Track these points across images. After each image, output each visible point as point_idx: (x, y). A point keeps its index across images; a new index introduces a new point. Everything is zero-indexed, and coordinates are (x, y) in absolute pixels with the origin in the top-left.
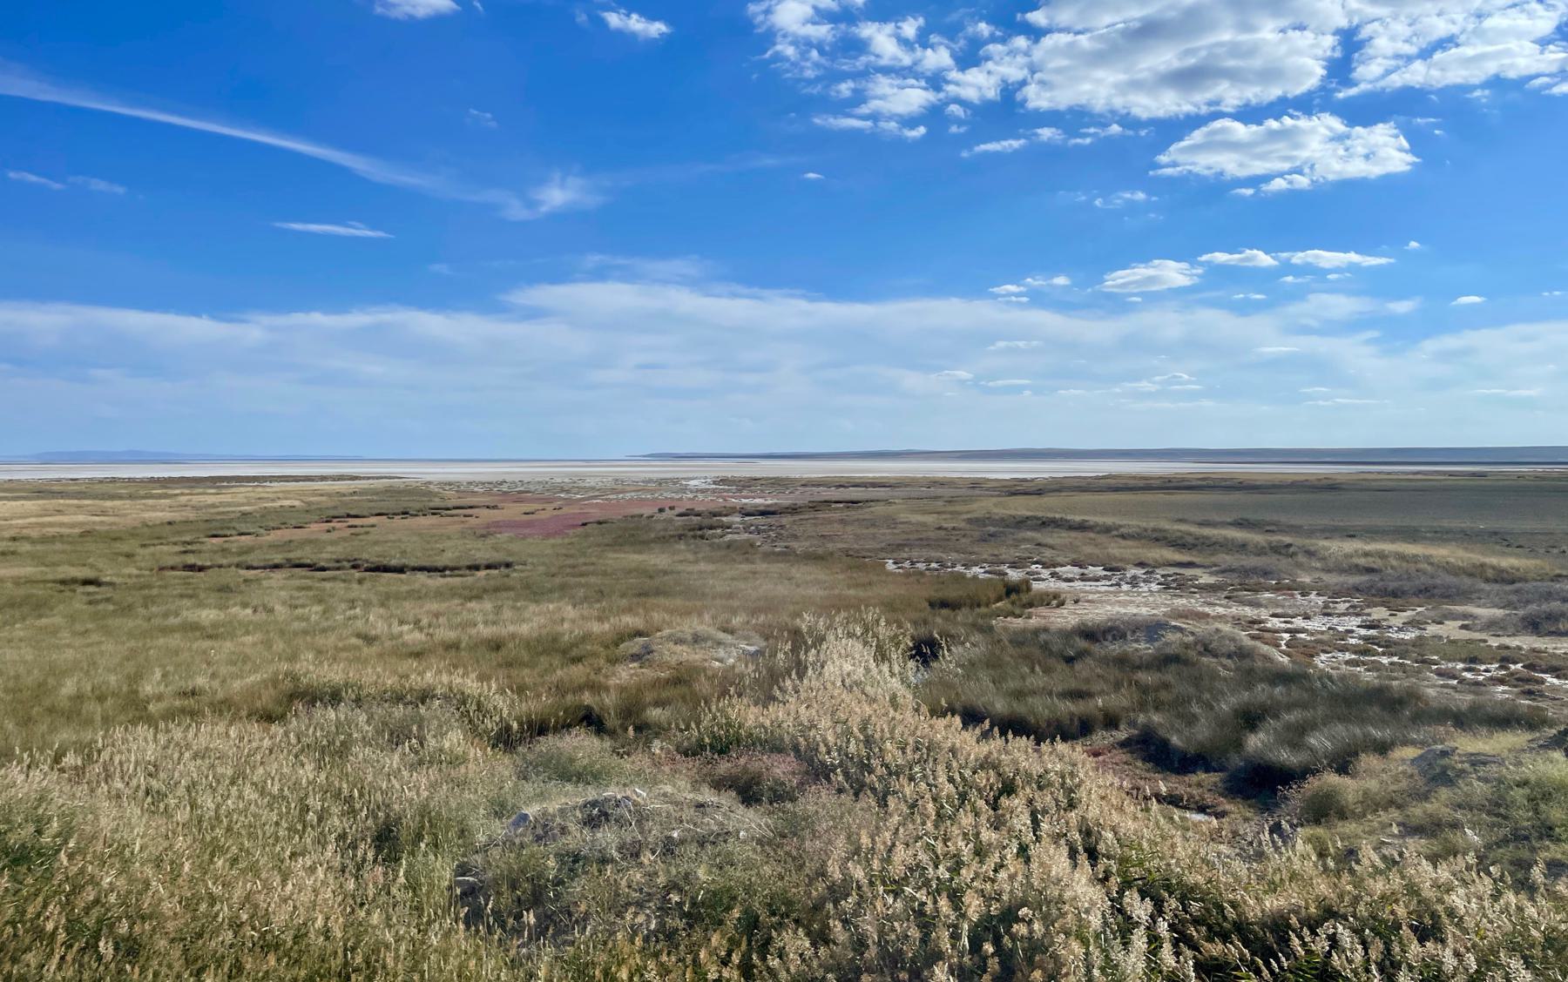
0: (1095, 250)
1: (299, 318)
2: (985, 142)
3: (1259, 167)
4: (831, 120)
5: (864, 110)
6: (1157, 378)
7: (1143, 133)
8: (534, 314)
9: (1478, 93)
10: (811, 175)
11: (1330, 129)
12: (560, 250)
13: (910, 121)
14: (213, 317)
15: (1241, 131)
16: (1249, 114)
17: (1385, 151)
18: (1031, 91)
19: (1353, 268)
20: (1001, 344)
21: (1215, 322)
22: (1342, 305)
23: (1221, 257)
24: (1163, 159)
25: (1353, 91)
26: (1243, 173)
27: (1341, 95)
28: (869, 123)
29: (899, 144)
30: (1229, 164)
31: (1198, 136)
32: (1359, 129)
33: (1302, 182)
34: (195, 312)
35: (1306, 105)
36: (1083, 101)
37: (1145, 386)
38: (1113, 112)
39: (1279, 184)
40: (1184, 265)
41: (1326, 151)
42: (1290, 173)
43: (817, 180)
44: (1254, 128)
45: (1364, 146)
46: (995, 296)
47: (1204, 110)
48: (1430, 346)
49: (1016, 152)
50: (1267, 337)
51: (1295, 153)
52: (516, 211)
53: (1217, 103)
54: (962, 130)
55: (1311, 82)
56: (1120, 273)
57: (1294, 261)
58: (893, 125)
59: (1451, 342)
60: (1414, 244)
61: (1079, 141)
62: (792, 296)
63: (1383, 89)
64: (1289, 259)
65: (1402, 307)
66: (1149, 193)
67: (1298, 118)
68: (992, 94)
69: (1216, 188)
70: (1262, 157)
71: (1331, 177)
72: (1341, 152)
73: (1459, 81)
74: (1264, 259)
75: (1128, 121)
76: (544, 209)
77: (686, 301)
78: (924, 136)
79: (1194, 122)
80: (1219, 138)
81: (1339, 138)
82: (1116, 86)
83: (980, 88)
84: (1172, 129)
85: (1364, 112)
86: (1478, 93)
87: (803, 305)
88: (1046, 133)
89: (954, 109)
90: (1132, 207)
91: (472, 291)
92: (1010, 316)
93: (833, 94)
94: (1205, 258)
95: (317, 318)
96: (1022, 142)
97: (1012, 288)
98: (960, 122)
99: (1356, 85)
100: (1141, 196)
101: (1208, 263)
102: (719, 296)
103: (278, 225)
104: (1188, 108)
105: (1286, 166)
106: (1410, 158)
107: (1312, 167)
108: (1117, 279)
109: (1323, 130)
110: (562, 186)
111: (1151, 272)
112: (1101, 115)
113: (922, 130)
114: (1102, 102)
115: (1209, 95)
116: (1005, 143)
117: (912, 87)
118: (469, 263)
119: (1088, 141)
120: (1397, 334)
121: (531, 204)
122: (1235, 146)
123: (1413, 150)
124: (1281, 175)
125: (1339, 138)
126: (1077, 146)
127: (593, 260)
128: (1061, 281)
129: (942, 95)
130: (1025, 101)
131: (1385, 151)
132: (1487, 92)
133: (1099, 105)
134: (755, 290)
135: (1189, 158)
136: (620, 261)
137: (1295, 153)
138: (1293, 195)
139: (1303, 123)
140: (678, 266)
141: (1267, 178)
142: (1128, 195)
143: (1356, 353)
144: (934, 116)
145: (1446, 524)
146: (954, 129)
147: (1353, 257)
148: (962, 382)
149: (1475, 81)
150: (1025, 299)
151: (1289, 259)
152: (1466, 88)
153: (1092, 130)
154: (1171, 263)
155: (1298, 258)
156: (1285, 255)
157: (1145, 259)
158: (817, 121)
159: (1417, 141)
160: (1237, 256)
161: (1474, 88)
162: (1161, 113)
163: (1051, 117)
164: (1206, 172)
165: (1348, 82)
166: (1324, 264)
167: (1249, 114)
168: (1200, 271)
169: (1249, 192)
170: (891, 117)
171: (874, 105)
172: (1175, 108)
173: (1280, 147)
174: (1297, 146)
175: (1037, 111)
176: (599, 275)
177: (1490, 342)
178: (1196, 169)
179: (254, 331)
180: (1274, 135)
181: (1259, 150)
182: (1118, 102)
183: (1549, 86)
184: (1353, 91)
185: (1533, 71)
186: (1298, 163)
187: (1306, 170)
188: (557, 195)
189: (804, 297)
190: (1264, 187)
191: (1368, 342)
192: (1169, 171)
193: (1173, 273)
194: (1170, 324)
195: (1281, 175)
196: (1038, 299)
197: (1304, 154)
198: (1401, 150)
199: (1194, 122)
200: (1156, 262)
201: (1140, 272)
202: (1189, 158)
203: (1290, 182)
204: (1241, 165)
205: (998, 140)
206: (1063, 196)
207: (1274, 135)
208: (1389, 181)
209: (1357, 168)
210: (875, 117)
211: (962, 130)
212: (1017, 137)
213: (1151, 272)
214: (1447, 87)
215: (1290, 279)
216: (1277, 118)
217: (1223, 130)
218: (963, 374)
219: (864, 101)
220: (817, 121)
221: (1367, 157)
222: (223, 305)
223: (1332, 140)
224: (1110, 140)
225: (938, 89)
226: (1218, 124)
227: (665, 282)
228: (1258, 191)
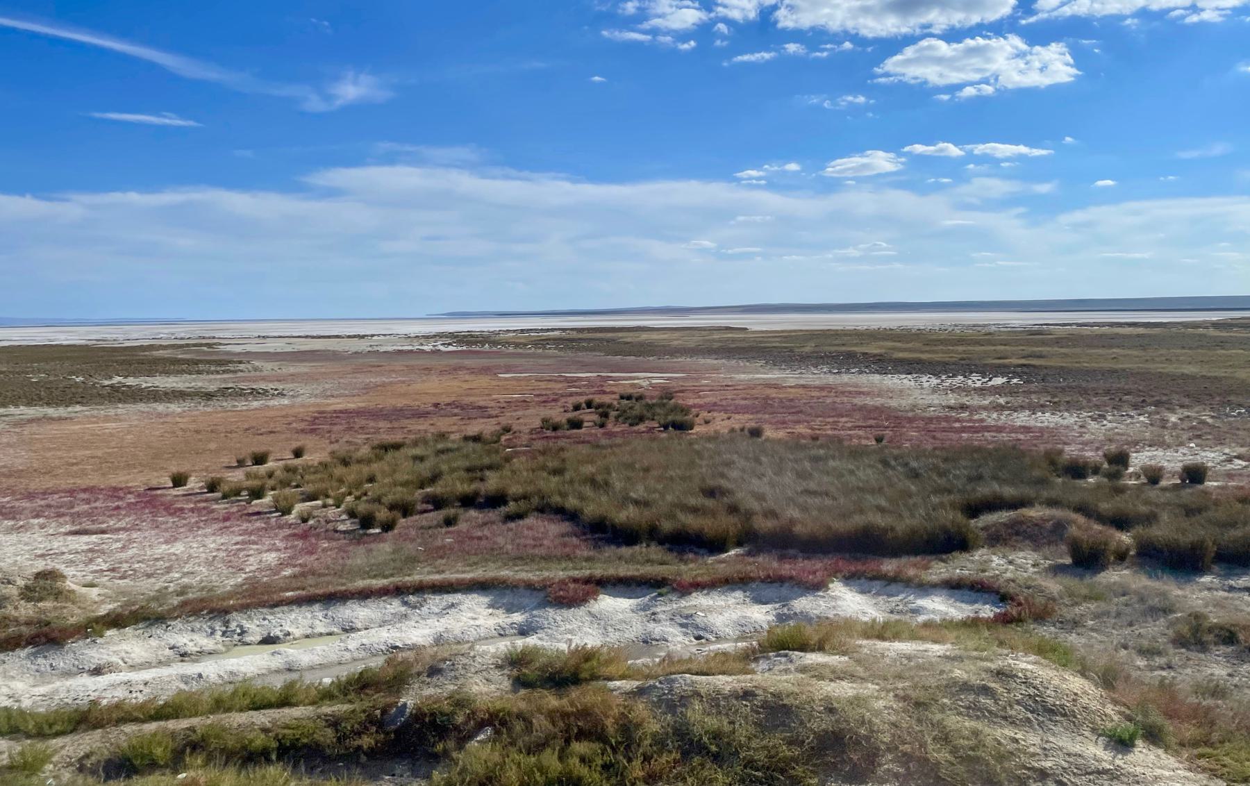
0: (822, 141)
1: (116, 197)
2: (741, 54)
3: (955, 77)
4: (617, 33)
5: (646, 26)
6: (861, 246)
7: (869, 49)
8: (332, 193)
9: (1129, 21)
10: (597, 78)
11: (1016, 48)
12: (357, 135)
13: (683, 36)
14: (36, 197)
15: (943, 48)
16: (952, 35)
17: (1055, 66)
18: (781, 13)
19: (1021, 158)
20: (741, 218)
21: (904, 202)
22: (999, 187)
23: (919, 148)
24: (878, 70)
25: (1032, 20)
26: (942, 82)
27: (1023, 22)
28: (649, 37)
29: (675, 52)
30: (931, 74)
31: (909, 52)
32: (1038, 48)
33: (988, 90)
34: (21, 193)
35: (998, 29)
36: (822, 22)
37: (852, 252)
38: (846, 32)
39: (969, 91)
40: (892, 155)
41: (1013, 65)
42: (979, 83)
43: (601, 83)
44: (955, 46)
45: (1040, 61)
46: (739, 180)
47: (918, 31)
48: (1065, 219)
49: (768, 62)
50: (936, 209)
51: (988, 66)
52: (314, 104)
53: (929, 26)
54: (725, 43)
55: (1006, 10)
56: (839, 161)
57: (976, 152)
58: (668, 39)
59: (1079, 216)
60: (1068, 139)
61: (818, 54)
62: (555, 178)
63: (1057, 18)
64: (972, 150)
65: (1044, 188)
66: (868, 97)
67: (989, 38)
68: (752, 15)
69: (921, 93)
70: (959, 70)
71: (1010, 86)
72: (1022, 66)
73: (1114, 11)
74: (953, 150)
75: (856, 38)
76: (339, 103)
77: (466, 182)
78: (694, 49)
79: (909, 40)
80: (927, 53)
81: (1020, 55)
82: (850, 10)
83: (743, 9)
84: (893, 45)
85: (1040, 35)
86: (1129, 21)
87: (567, 186)
88: (792, 48)
89: (722, 27)
90: (855, 109)
91: (282, 177)
92: (756, 195)
93: (620, 11)
94: (907, 149)
95: (134, 197)
96: (772, 54)
97: (753, 173)
98: (724, 38)
99: (1036, 13)
100: (861, 99)
101: (909, 153)
102: (494, 178)
103: (97, 115)
104: (904, 30)
105: (977, 77)
106: (1074, 71)
107: (996, 79)
108: (842, 166)
109: (1009, 49)
110: (355, 83)
111: (865, 160)
112: (836, 35)
113: (692, 43)
114: (838, 23)
115: (923, 20)
116: (758, 55)
117: (688, 7)
118: (291, 151)
119: (825, 54)
120: (1039, 209)
121: (328, 98)
122: (940, 60)
123: (1077, 65)
124: (971, 84)
125: (1020, 55)
126: (817, 59)
127: (384, 146)
128: (793, 167)
129: (712, 15)
130: (776, 22)
131: (1055, 66)
132: (1136, 21)
133: (834, 26)
134: (526, 173)
135: (902, 67)
136: (408, 148)
137: (988, 66)
138: (980, 100)
139: (993, 42)
140: (462, 153)
141: (960, 87)
142: (850, 98)
143: (1008, 225)
144: (703, 32)
145: (1002, 348)
146: (718, 43)
147: (1022, 149)
148: (703, 251)
149: (1127, 12)
150: (763, 182)
151: (972, 150)
152: (1120, 17)
153: (828, 46)
154: (881, 153)
155: (980, 149)
156: (969, 147)
157: (859, 149)
158: (605, 33)
159: (1079, 58)
160: (932, 148)
161: (1125, 17)
162: (884, 34)
163: (796, 35)
164: (913, 82)
165: (1032, 12)
166: (999, 155)
167: (952, 35)
168: (903, 160)
169: (946, 97)
170: (669, 32)
171: (657, 22)
172: (895, 30)
173: (976, 61)
174: (989, 60)
175: (784, 30)
176: (390, 159)
177: (1109, 217)
178: (905, 79)
179: (73, 208)
180: (972, 51)
181: (957, 64)
182: (850, 25)
183: (1183, 17)
184: (1032, 20)
185: (1172, 5)
186: (987, 74)
187: (992, 81)
188: (352, 89)
189: (567, 179)
190: (958, 94)
191: (1018, 216)
192: (882, 80)
193: (882, 161)
194: (864, 202)
195: (971, 84)
196: (772, 185)
197: (993, 67)
198: (1067, 64)
199: (909, 40)
200: (869, 152)
201: (855, 161)
202: (902, 67)
203: (979, 90)
204: (941, 75)
205: (752, 52)
206: (778, 95)
207: (972, 51)
208: (1055, 89)
209: (1034, 79)
210: (655, 32)
211: (725, 43)
212: (768, 50)
213: (865, 160)
214: (1106, 17)
215: (971, 166)
216: (973, 38)
217: (930, 48)
218: (707, 243)
219: (646, 19)
220: (605, 33)
221: (1041, 70)
222: (42, 188)
223: (1017, 56)
224: (845, 53)
225: (709, 10)
226: (924, 43)
227: (448, 166)
228: (953, 97)
